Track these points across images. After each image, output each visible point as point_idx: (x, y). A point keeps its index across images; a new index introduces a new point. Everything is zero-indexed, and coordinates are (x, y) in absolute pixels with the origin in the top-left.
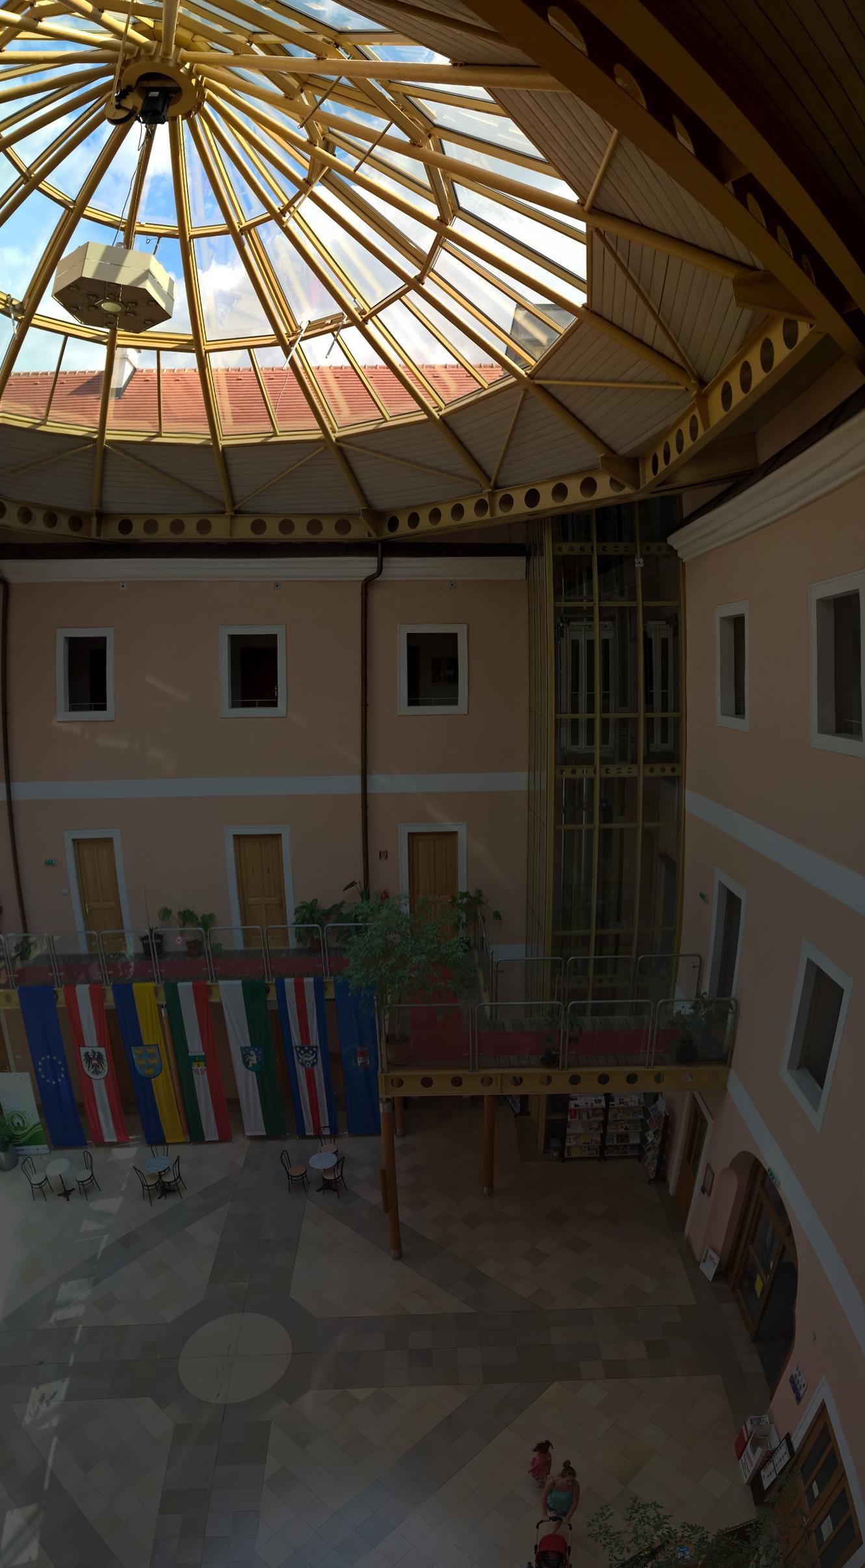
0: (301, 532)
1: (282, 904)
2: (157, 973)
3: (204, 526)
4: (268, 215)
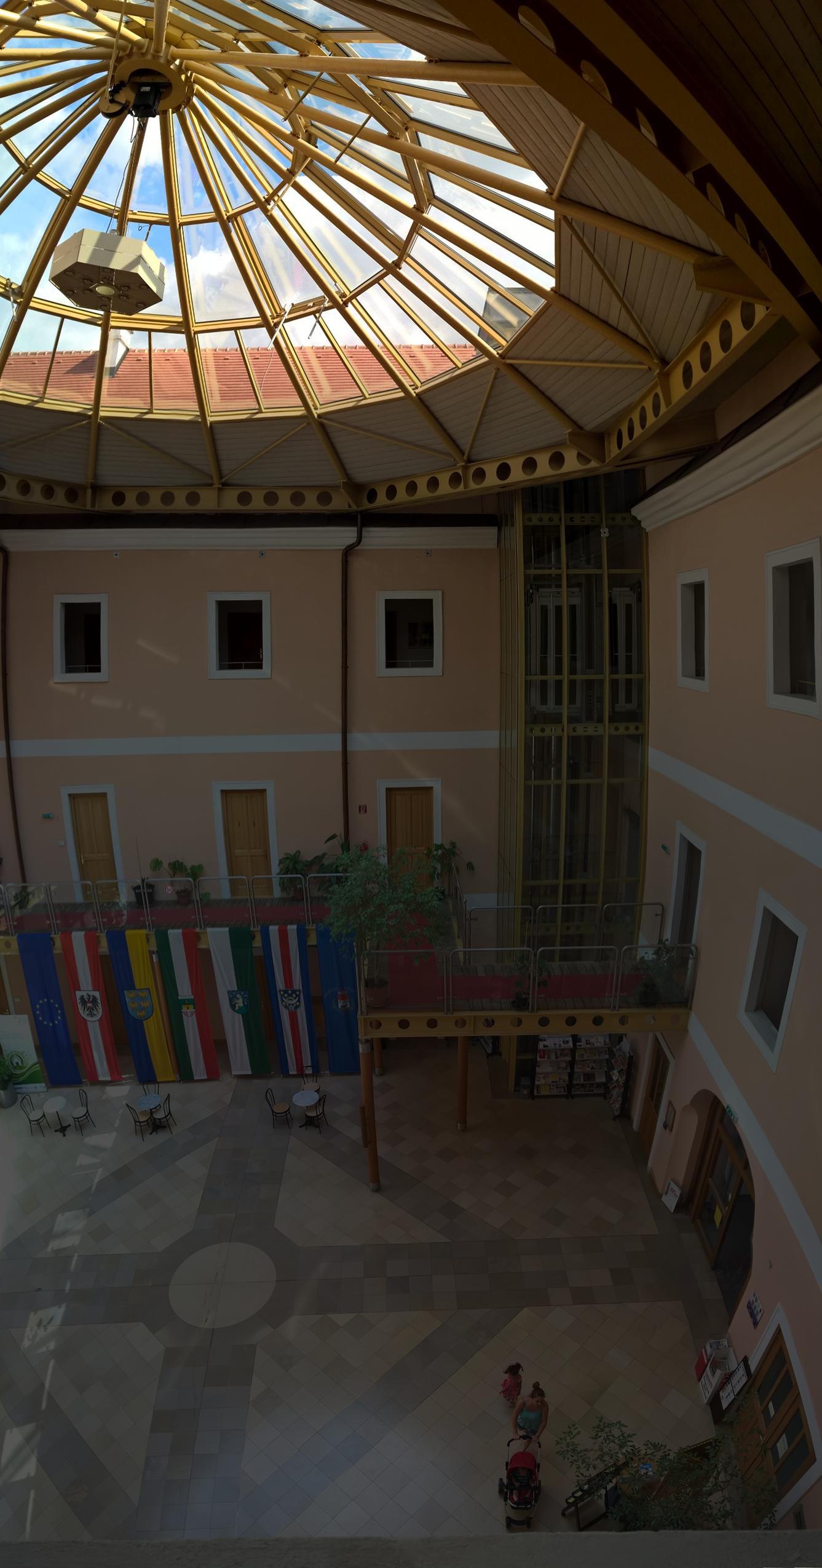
0: (285, 504)
1: (267, 856)
2: (148, 920)
3: (193, 498)
4: (254, 203)
